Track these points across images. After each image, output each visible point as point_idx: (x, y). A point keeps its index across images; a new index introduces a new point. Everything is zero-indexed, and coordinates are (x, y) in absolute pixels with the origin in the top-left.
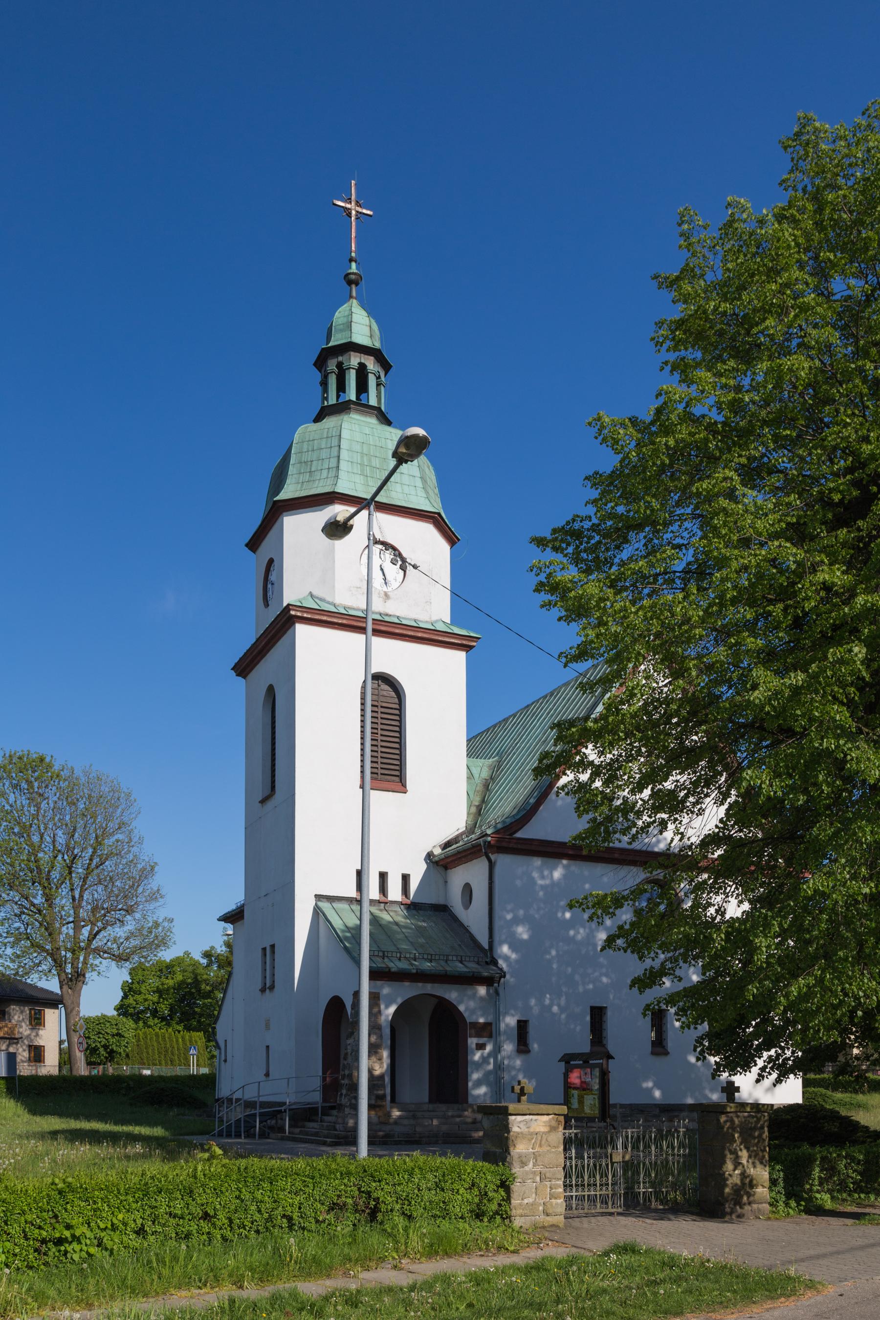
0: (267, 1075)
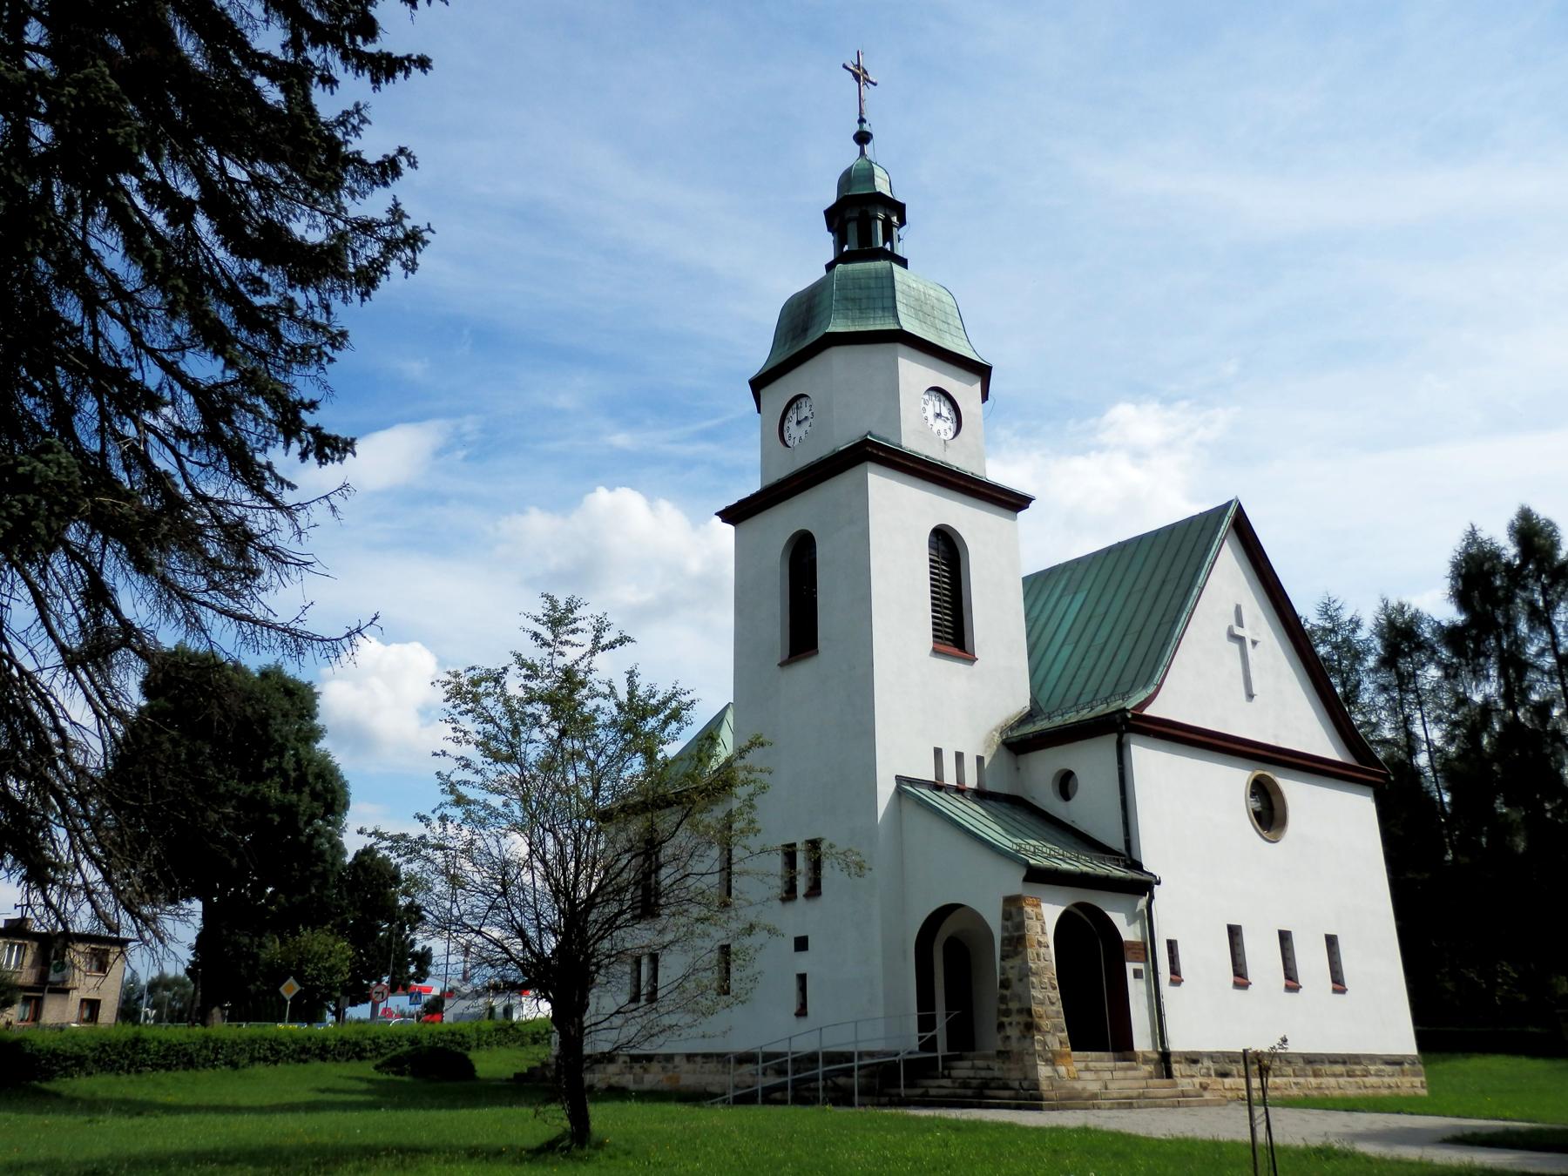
0: (802, 1012)
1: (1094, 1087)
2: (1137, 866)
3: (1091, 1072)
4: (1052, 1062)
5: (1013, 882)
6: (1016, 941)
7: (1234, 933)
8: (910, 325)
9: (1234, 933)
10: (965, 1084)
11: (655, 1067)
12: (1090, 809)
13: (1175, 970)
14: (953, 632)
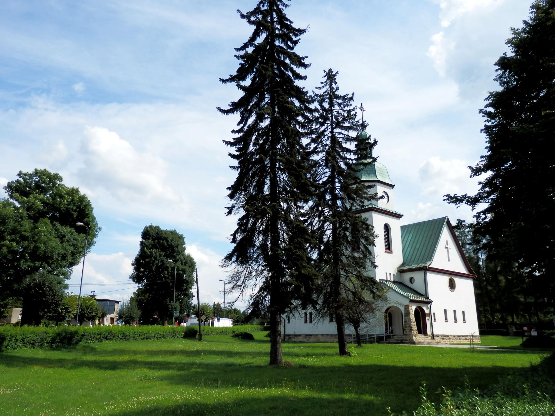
1: (422, 341)
2: (428, 298)
3: (419, 338)
4: (415, 336)
5: (407, 302)
6: (408, 314)
7: (445, 311)
8: (380, 179)
9: (445, 311)
10: (398, 340)
11: (313, 337)
12: (418, 285)
13: (435, 319)
14: (388, 247)
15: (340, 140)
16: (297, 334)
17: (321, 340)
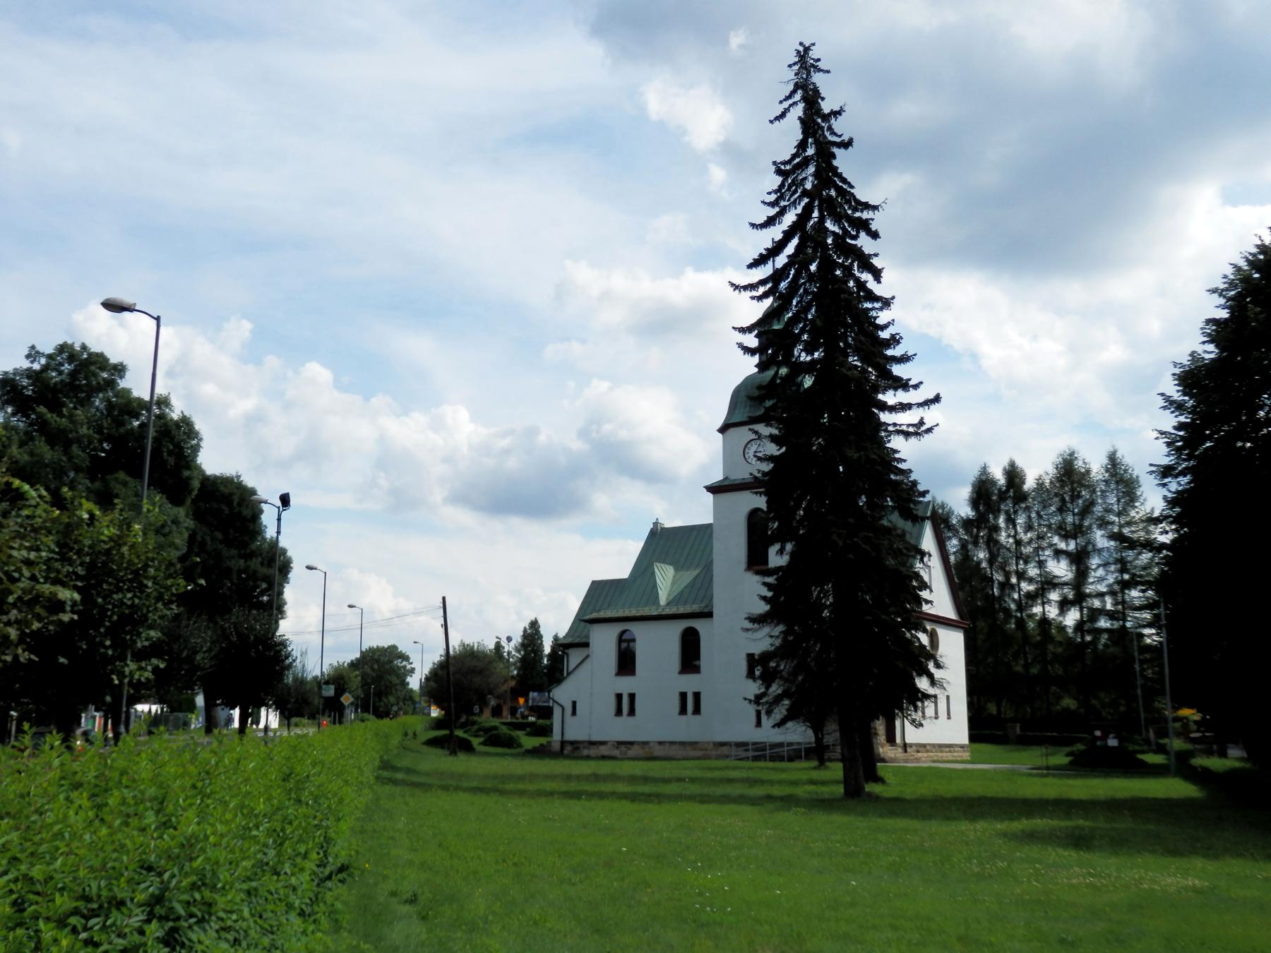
11: (636, 747)
15: (809, 358)
16: (595, 738)
17: (656, 753)
